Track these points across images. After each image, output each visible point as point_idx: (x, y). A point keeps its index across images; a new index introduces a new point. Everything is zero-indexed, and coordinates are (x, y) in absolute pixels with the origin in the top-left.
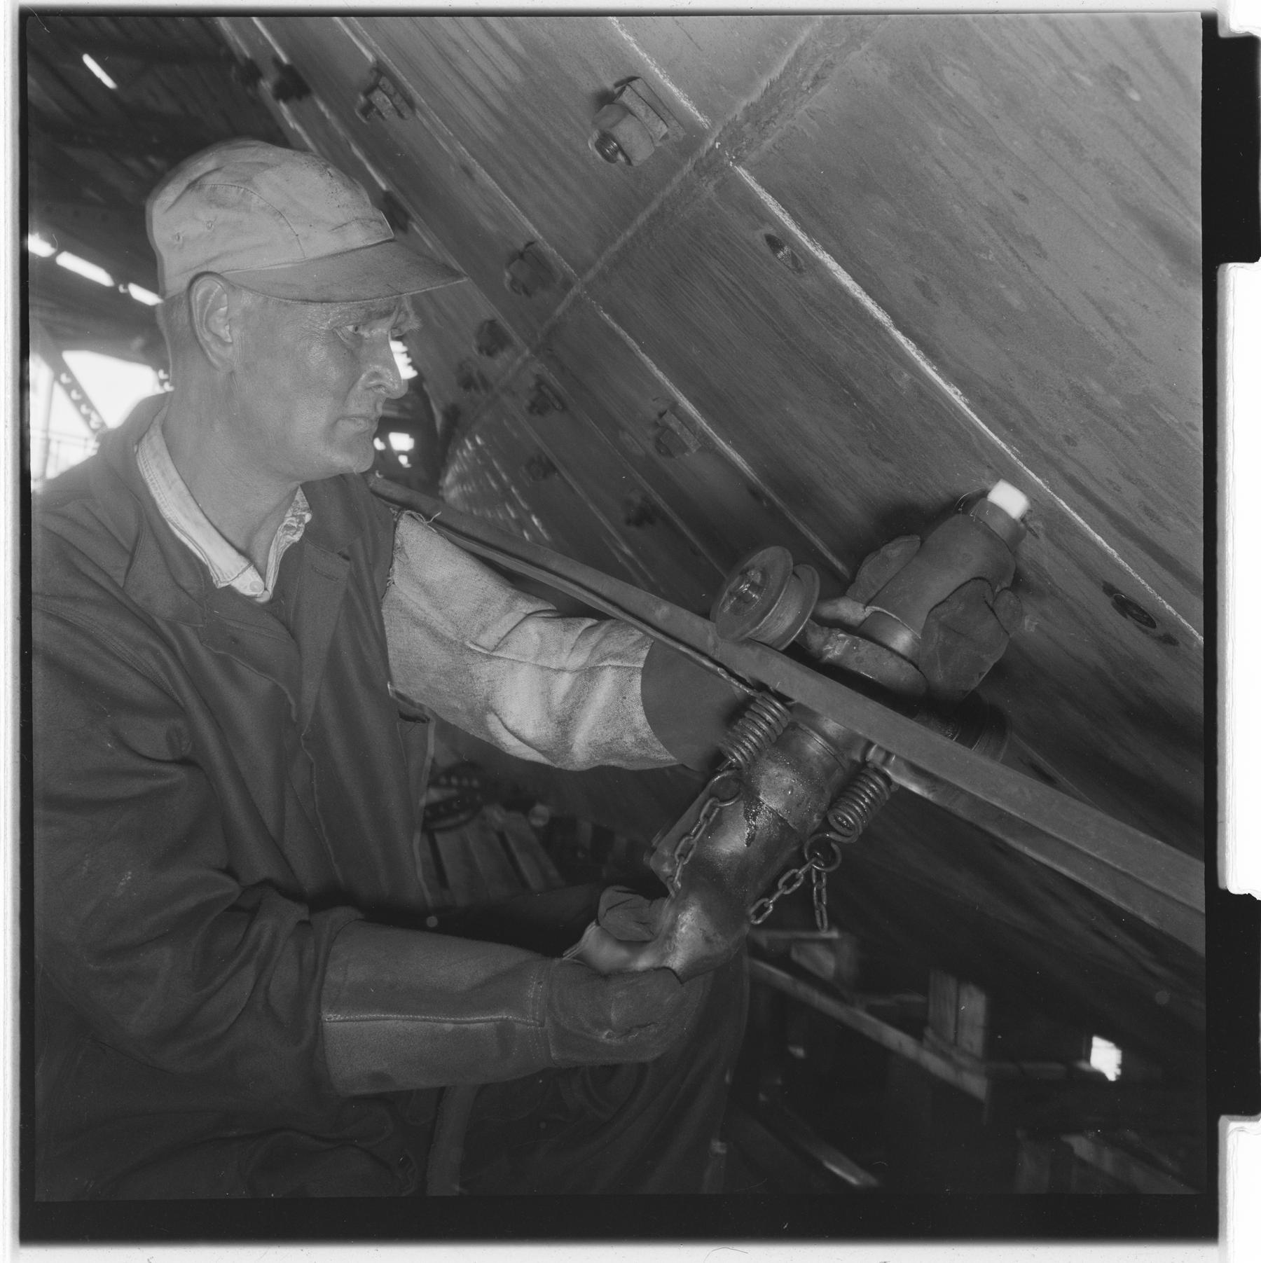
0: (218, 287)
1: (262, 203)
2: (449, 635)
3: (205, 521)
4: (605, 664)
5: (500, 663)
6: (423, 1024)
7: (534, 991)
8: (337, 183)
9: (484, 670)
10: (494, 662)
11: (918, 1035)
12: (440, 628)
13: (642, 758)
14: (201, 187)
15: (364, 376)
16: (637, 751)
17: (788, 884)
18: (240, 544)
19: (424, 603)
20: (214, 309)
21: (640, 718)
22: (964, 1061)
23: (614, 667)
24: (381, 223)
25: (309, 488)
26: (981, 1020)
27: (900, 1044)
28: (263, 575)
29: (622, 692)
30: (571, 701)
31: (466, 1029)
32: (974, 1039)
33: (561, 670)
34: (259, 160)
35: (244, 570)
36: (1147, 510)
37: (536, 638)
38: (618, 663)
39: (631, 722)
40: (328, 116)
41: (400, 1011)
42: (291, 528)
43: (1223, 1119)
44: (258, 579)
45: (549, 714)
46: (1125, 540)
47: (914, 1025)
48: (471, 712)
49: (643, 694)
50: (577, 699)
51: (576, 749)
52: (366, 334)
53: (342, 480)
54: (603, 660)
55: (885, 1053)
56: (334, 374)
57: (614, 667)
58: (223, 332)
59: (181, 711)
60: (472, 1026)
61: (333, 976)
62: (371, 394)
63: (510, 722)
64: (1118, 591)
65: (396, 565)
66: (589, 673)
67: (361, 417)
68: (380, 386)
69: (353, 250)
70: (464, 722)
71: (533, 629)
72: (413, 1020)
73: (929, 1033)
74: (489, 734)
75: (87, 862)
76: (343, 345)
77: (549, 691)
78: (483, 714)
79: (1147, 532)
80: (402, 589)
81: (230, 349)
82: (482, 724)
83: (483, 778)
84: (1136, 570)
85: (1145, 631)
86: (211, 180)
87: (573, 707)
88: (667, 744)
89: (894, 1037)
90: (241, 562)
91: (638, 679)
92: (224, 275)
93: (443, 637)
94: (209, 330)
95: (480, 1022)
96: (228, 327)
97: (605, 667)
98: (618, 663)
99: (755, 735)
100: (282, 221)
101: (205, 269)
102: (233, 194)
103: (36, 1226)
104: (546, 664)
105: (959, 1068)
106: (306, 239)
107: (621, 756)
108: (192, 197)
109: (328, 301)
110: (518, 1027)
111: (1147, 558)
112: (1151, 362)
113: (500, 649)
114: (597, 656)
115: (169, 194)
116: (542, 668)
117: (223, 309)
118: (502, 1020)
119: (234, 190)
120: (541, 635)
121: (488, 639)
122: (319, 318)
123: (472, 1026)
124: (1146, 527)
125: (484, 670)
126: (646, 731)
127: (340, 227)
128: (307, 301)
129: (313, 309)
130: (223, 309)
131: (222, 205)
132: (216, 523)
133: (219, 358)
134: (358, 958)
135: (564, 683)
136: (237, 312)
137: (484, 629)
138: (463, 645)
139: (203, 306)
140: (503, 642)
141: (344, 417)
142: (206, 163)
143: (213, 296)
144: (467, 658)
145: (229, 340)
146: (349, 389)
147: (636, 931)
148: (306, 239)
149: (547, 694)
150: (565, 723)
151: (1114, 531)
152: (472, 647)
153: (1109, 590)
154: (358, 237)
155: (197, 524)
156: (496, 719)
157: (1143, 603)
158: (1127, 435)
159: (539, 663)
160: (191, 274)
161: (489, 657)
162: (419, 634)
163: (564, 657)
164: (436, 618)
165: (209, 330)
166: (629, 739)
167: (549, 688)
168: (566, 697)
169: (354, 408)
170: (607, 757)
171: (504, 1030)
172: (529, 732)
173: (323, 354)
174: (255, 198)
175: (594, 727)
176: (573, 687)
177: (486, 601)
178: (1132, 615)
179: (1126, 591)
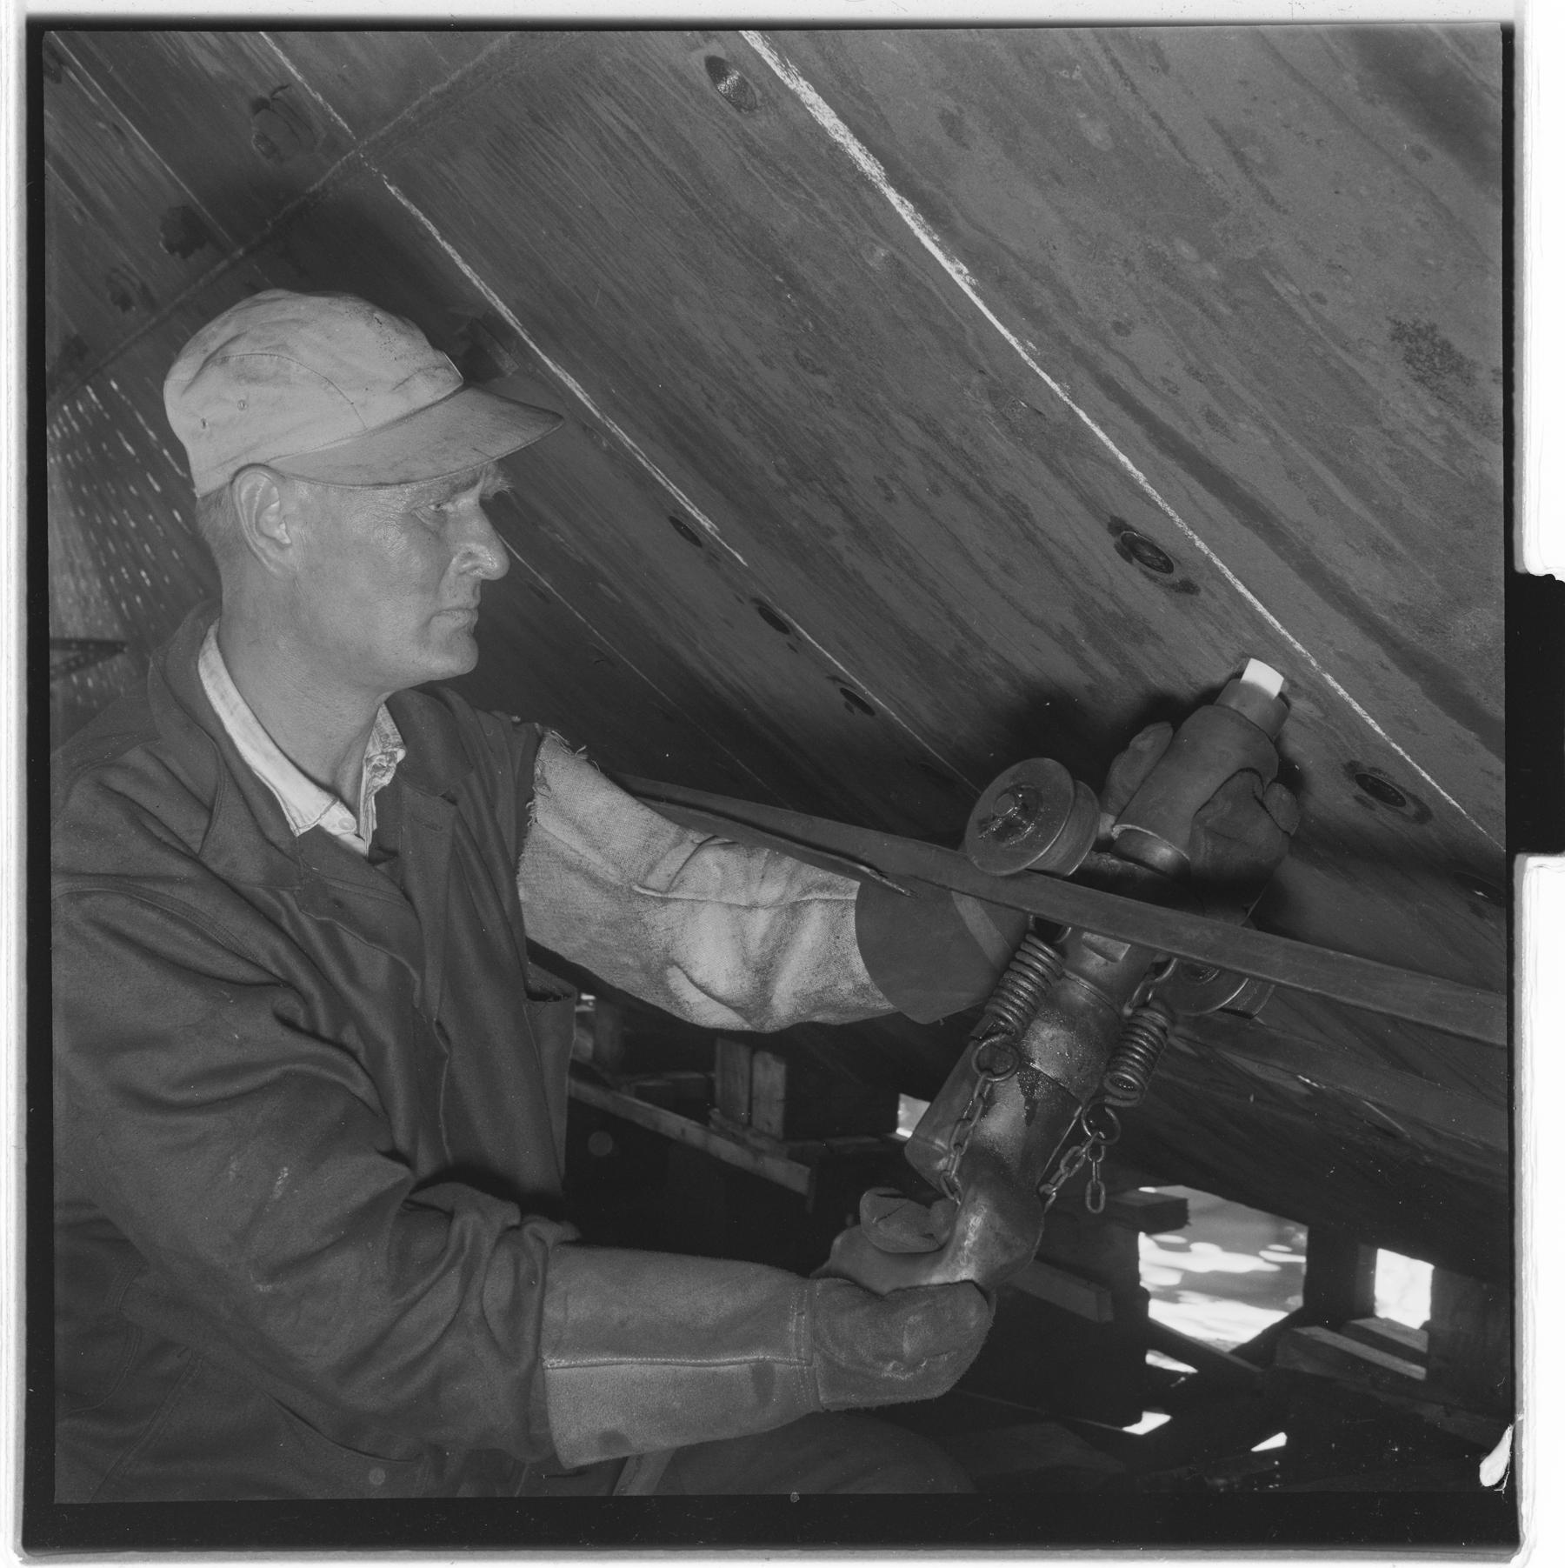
0: (263, 479)
1: (304, 371)
2: (612, 879)
3: (276, 752)
4: (810, 897)
5: (678, 906)
6: (666, 1368)
7: (796, 1325)
8: (389, 330)
9: (660, 919)
10: (671, 906)
11: (703, 1118)
12: (600, 874)
13: (859, 1008)
14: (225, 360)
15: (454, 560)
16: (855, 1001)
17: (1070, 1165)
18: (324, 777)
19: (577, 843)
20: (263, 507)
21: (858, 964)
22: (761, 1143)
23: (821, 901)
24: (448, 368)
25: (395, 706)
26: (780, 1094)
27: (683, 1131)
28: (352, 808)
29: (834, 930)
30: (771, 943)
31: (715, 1373)
32: (772, 1116)
33: (752, 907)
34: (290, 316)
35: (328, 809)
36: (1210, 417)
37: (716, 871)
38: (827, 896)
39: (846, 965)
40: (475, 282)
41: (636, 1353)
42: (383, 758)
43: (1519, 858)
44: (348, 815)
45: (745, 961)
46: (1169, 463)
47: (696, 1106)
48: (645, 969)
49: (858, 931)
50: (779, 945)
51: (775, 1001)
52: (449, 507)
53: (431, 690)
54: (805, 892)
55: (662, 1142)
56: (418, 564)
57: (821, 901)
58: (280, 532)
59: (289, 985)
60: (723, 1369)
61: (552, 1313)
62: (466, 579)
63: (698, 975)
64: (1131, 528)
65: (539, 800)
66: (794, 910)
67: (459, 608)
68: (476, 568)
69: (422, 410)
70: (630, 981)
71: (710, 857)
72: (652, 1364)
73: (715, 1113)
74: (670, 995)
75: (233, 1166)
76: (425, 528)
77: (743, 934)
78: (662, 970)
79: (1200, 447)
80: (547, 823)
81: (290, 552)
82: (661, 983)
83: (658, 1045)
84: (1166, 497)
85: (1153, 579)
86: (237, 350)
87: (773, 951)
88: (887, 990)
89: (674, 1123)
90: (323, 799)
91: (852, 913)
92: (273, 464)
93: (606, 883)
94: (262, 534)
95: (733, 1364)
96: (283, 526)
97: (810, 902)
98: (827, 896)
99: (1035, 970)
100: (332, 389)
101: (243, 462)
102: (267, 365)
103: (42, 1524)
104: (734, 900)
105: (758, 1153)
106: (363, 406)
107: (832, 1007)
108: (215, 375)
109: (406, 482)
110: (777, 1367)
111: (1193, 482)
112: (1285, 212)
113: (676, 889)
114: (798, 888)
115: (181, 372)
116: (730, 906)
117: (275, 505)
118: (758, 1361)
119: (266, 359)
120: (722, 867)
121: (657, 879)
122: (395, 501)
123: (723, 1369)
124: (1205, 440)
125: (660, 919)
126: (864, 977)
127: (401, 385)
128: (381, 485)
129: (384, 493)
130: (275, 505)
131: (255, 379)
132: (292, 756)
133: (278, 565)
134: (585, 1289)
135: (760, 923)
136: (292, 508)
137: (652, 867)
138: (631, 889)
139: (250, 508)
140: (676, 880)
141: (439, 613)
142: (217, 332)
143: (258, 493)
144: (638, 905)
145: (287, 541)
146: (440, 579)
147: (912, 1241)
148: (363, 406)
149: (740, 937)
150: (765, 972)
151: (1149, 448)
152: (642, 891)
153: (1117, 527)
154: (425, 392)
155: (267, 756)
156: (679, 972)
157: (1164, 542)
158: (1215, 318)
159: (724, 899)
160: (232, 469)
161: (665, 901)
162: (574, 881)
163: (754, 888)
164: (594, 859)
165: (262, 534)
166: (846, 986)
167: (748, 937)
168: (764, 939)
169: (450, 601)
170: (815, 1010)
171: (762, 1374)
172: (722, 987)
173: (404, 539)
174: (294, 366)
175: (799, 974)
176: (772, 927)
177: (653, 834)
178: (1141, 559)
179: (1143, 525)
